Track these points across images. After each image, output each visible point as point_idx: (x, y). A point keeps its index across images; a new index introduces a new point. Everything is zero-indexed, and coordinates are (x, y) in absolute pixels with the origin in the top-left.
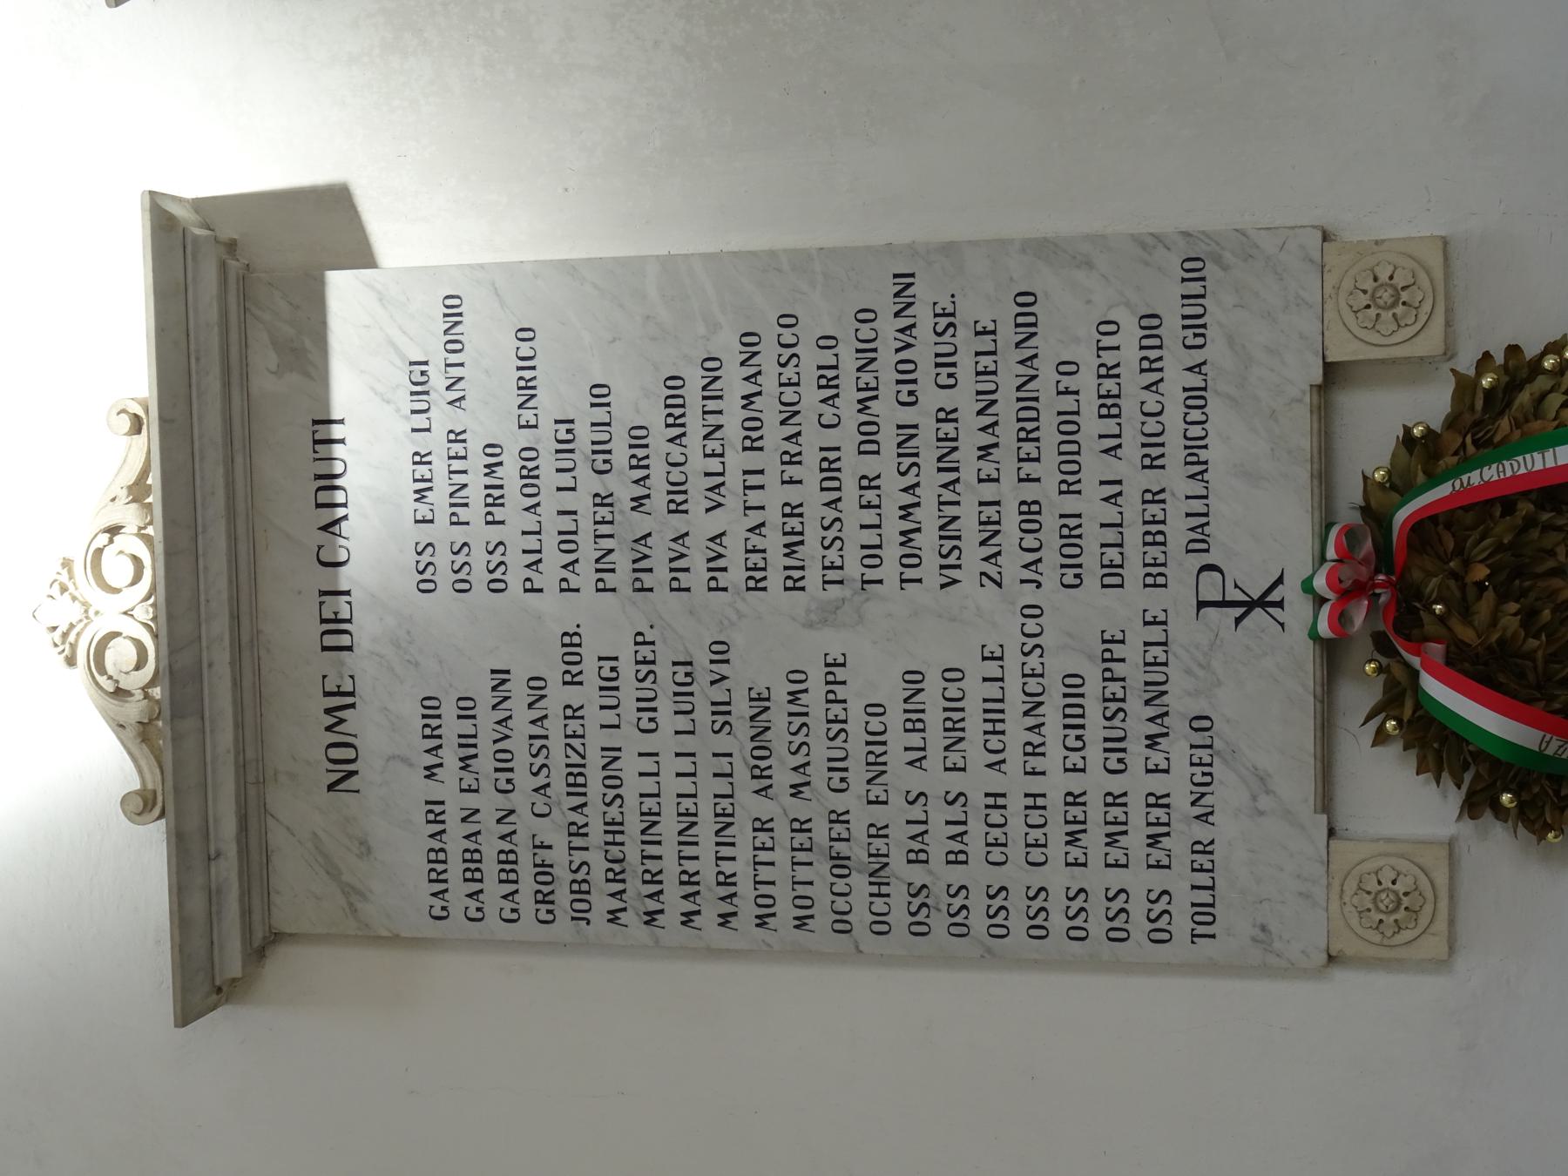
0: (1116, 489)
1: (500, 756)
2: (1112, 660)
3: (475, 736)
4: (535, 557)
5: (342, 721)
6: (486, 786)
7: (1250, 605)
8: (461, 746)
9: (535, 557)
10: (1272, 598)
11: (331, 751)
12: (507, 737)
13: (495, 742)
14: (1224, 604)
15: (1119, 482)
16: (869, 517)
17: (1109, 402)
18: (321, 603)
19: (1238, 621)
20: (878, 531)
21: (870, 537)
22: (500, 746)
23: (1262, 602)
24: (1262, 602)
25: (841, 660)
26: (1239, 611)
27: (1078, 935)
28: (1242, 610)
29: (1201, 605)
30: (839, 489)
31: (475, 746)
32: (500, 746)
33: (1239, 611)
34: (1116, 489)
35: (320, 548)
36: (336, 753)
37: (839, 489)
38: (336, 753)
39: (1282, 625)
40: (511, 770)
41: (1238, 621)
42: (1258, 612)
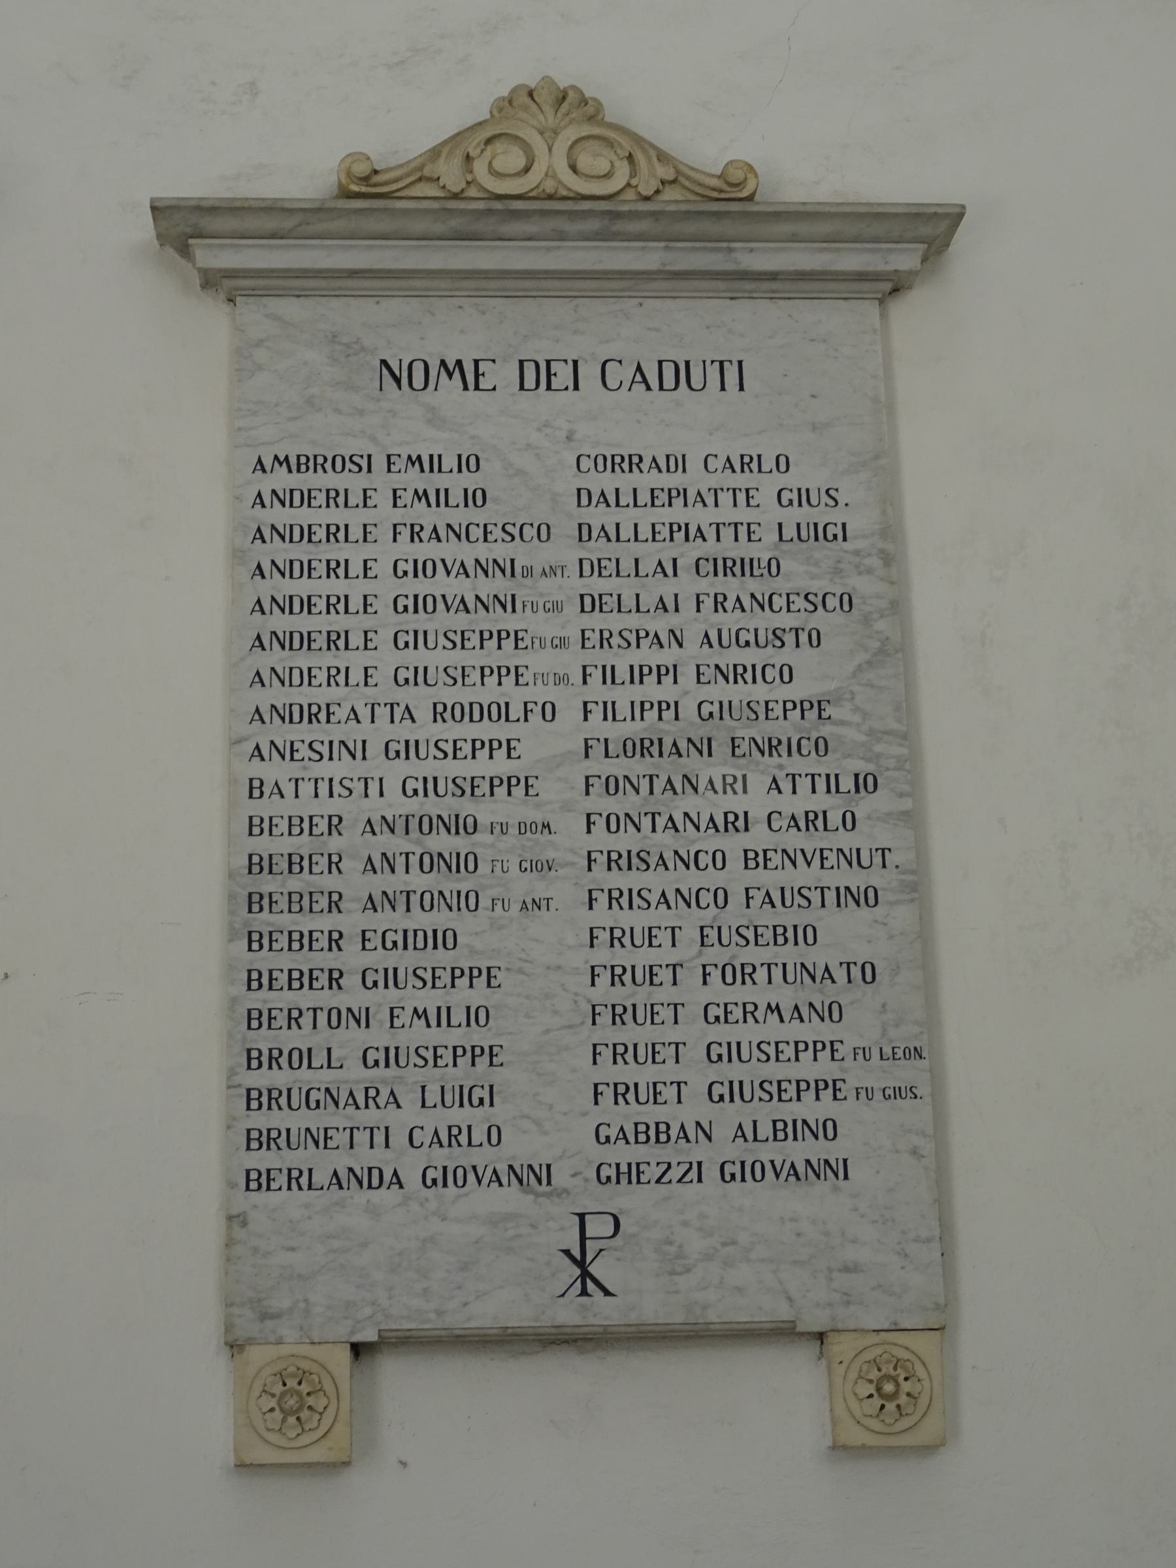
0: (670, 571)
1: (429, 565)
2: (500, 639)
3: (447, 505)
4: (612, 499)
5: (450, 375)
6: (398, 515)
7: (581, 1264)
8: (431, 456)
9: (612, 499)
10: (590, 1285)
11: (422, 365)
12: (448, 573)
13: (443, 561)
14: (583, 1239)
15: (675, 574)
16: (645, 532)
17: (761, 859)
18: (565, 361)
19: (567, 1252)
20: (633, 539)
21: (627, 532)
22: (440, 566)
23: (585, 1275)
24: (585, 1275)
25: (513, 754)
26: (576, 1253)
27: (254, 826)
28: (579, 1258)
29: (582, 1217)
30: (668, 470)
31: (438, 505)
32: (440, 566)
33: (576, 1253)
34: (670, 571)
35: (620, 362)
36: (418, 368)
37: (668, 470)
38: (418, 368)
39: (563, 1295)
40: (416, 575)
41: (567, 1252)
42: (578, 1272)
